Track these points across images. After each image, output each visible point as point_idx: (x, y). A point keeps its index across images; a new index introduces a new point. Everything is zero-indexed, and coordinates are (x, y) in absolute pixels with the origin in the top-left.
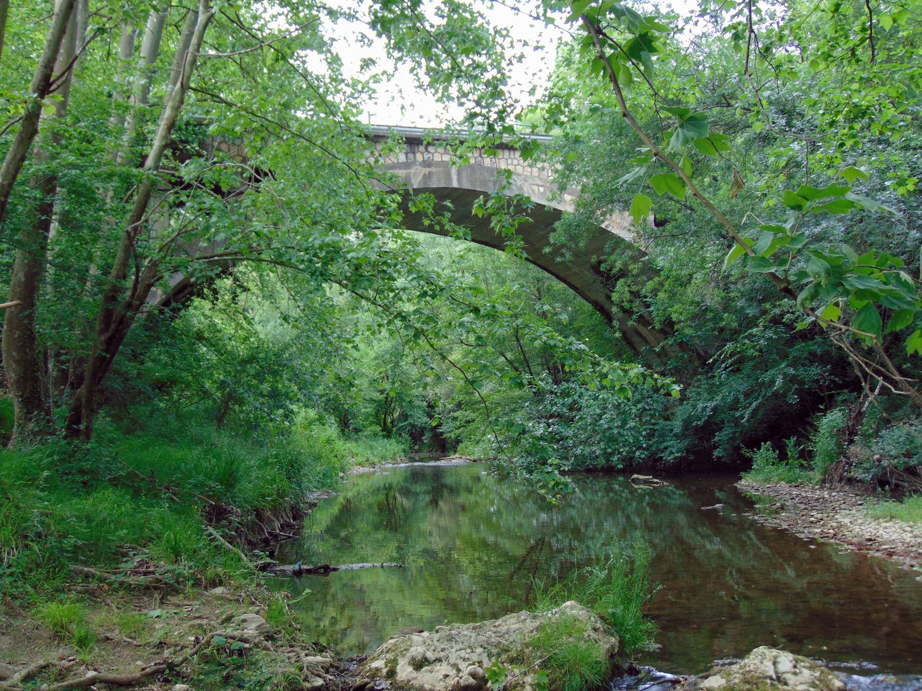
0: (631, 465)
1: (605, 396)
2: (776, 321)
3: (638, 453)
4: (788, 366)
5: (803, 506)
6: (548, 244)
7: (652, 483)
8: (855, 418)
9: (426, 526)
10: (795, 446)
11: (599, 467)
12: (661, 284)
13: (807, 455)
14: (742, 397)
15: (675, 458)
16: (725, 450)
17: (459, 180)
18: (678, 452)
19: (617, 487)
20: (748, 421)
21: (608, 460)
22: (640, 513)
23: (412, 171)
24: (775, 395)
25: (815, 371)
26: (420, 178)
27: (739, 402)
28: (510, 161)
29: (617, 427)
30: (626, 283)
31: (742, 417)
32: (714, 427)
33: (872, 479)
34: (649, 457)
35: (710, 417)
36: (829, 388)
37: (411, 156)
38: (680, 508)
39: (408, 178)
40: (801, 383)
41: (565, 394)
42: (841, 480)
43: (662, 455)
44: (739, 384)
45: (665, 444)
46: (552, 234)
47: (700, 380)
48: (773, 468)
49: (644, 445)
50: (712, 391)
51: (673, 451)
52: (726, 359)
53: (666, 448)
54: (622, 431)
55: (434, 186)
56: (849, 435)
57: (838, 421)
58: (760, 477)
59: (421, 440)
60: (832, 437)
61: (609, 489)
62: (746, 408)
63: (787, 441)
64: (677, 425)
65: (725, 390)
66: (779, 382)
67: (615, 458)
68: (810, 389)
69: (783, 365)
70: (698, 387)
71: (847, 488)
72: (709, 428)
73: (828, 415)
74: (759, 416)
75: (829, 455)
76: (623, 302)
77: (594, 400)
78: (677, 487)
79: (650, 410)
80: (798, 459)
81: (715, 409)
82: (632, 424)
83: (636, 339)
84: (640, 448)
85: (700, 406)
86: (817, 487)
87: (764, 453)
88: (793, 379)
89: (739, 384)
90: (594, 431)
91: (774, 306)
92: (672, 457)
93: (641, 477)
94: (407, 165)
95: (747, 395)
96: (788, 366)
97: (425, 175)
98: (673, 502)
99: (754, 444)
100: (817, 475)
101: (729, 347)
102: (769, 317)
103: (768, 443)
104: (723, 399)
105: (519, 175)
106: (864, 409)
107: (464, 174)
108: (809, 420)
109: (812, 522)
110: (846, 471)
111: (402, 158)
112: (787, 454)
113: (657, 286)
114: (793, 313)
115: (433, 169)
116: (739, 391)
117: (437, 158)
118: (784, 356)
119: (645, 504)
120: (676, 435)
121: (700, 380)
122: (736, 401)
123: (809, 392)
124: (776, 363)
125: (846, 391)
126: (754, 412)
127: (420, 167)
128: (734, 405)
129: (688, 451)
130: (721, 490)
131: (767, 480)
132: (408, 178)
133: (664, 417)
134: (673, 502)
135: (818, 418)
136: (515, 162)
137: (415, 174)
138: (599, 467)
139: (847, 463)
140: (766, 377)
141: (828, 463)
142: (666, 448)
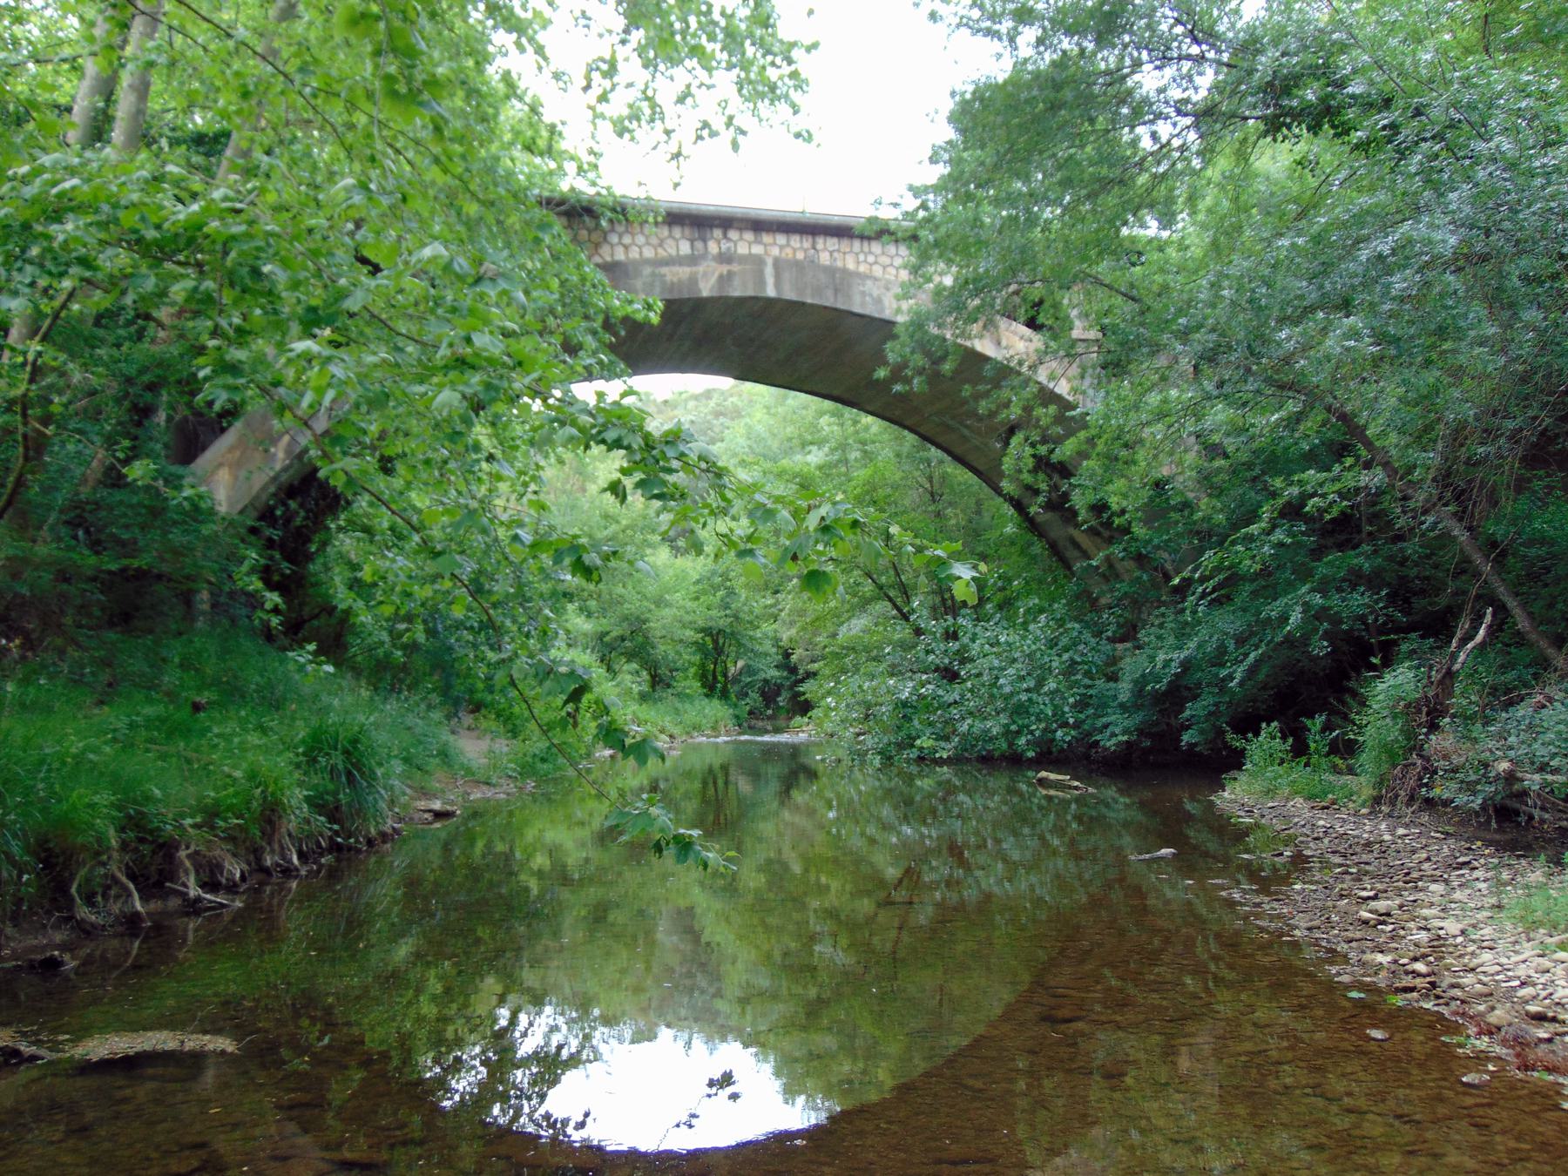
0: (1050, 753)
1: (1011, 639)
2: (1292, 511)
3: (1059, 733)
4: (1312, 590)
5: (1337, 860)
6: (885, 363)
7: (1070, 787)
8: (1441, 682)
9: (767, 828)
10: (1323, 730)
11: (997, 754)
12: (1091, 441)
13: (1346, 749)
14: (1231, 645)
15: (1118, 744)
16: (1202, 732)
17: (777, 285)
18: (1124, 733)
19: (1024, 787)
20: (1241, 684)
21: (1011, 744)
22: (1059, 830)
23: (701, 269)
24: (1289, 641)
25: (1359, 600)
26: (713, 280)
27: (1225, 653)
28: (862, 257)
29: (1028, 690)
30: (1026, 440)
31: (1231, 677)
32: (1186, 693)
33: (1484, 807)
34: (1077, 740)
35: (1176, 675)
36: (1382, 630)
37: (699, 245)
38: (1126, 824)
39: (693, 281)
40: (1336, 621)
41: (952, 636)
42: (1412, 799)
43: (1098, 738)
44: (1228, 622)
45: (1104, 720)
46: (889, 345)
47: (1163, 615)
48: (1281, 770)
49: (1071, 721)
50: (1183, 633)
51: (1116, 732)
52: (1203, 579)
53: (1106, 726)
54: (1034, 696)
55: (737, 293)
56: (1428, 714)
57: (1407, 687)
58: (1257, 786)
59: (776, 702)
60: (1395, 717)
61: (1012, 790)
62: (1238, 662)
63: (1308, 723)
64: (1124, 690)
65: (1204, 632)
66: (1295, 617)
67: (1022, 741)
68: (1351, 630)
69: (1304, 590)
70: (1161, 626)
71: (1425, 818)
72: (1177, 693)
73: (1387, 676)
74: (1261, 676)
75: (1388, 750)
76: (1020, 471)
77: (991, 645)
78: (1121, 791)
79: (1083, 663)
80: (1328, 755)
81: (1186, 665)
82: (1051, 685)
83: (1071, 553)
84: (1065, 725)
85: (1161, 657)
86: (1364, 811)
87: (1267, 742)
88: (1321, 614)
89: (1228, 622)
90: (992, 696)
91: (1291, 484)
92: (1114, 741)
93: (1053, 776)
94: (692, 260)
95: (1241, 641)
96: (1312, 590)
97: (721, 277)
98: (1112, 814)
99: (1248, 724)
100: (1363, 786)
101: (1209, 558)
102: (1280, 501)
103: (1275, 724)
104: (1200, 646)
105: (876, 279)
106: (1457, 667)
107: (786, 276)
108: (1352, 684)
109: (1366, 922)
110: (1426, 785)
111: (685, 248)
112: (1308, 747)
113: (1084, 447)
114: (1324, 496)
115: (735, 267)
116: (1227, 634)
117: (742, 249)
118: (1304, 574)
119: (1069, 817)
120: (1122, 706)
121: (1163, 615)
122: (1222, 650)
123: (1349, 637)
124: (1291, 586)
125: (1413, 635)
126: (1252, 671)
127: (713, 264)
128: (1219, 657)
129: (1141, 732)
130: (1192, 799)
131: (1269, 792)
132: (693, 281)
133: (1106, 675)
134: (1112, 814)
135: (1368, 681)
136: (871, 259)
137: (705, 274)
138: (997, 754)
139: (1425, 768)
140: (1273, 610)
141: (1385, 767)
142: (1106, 726)
